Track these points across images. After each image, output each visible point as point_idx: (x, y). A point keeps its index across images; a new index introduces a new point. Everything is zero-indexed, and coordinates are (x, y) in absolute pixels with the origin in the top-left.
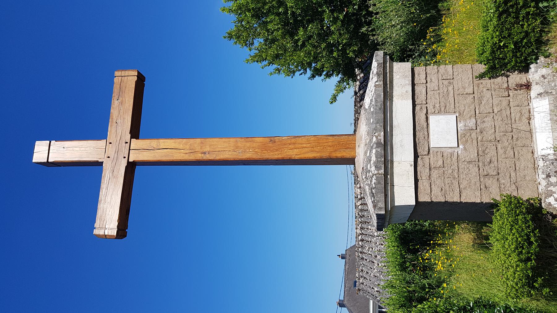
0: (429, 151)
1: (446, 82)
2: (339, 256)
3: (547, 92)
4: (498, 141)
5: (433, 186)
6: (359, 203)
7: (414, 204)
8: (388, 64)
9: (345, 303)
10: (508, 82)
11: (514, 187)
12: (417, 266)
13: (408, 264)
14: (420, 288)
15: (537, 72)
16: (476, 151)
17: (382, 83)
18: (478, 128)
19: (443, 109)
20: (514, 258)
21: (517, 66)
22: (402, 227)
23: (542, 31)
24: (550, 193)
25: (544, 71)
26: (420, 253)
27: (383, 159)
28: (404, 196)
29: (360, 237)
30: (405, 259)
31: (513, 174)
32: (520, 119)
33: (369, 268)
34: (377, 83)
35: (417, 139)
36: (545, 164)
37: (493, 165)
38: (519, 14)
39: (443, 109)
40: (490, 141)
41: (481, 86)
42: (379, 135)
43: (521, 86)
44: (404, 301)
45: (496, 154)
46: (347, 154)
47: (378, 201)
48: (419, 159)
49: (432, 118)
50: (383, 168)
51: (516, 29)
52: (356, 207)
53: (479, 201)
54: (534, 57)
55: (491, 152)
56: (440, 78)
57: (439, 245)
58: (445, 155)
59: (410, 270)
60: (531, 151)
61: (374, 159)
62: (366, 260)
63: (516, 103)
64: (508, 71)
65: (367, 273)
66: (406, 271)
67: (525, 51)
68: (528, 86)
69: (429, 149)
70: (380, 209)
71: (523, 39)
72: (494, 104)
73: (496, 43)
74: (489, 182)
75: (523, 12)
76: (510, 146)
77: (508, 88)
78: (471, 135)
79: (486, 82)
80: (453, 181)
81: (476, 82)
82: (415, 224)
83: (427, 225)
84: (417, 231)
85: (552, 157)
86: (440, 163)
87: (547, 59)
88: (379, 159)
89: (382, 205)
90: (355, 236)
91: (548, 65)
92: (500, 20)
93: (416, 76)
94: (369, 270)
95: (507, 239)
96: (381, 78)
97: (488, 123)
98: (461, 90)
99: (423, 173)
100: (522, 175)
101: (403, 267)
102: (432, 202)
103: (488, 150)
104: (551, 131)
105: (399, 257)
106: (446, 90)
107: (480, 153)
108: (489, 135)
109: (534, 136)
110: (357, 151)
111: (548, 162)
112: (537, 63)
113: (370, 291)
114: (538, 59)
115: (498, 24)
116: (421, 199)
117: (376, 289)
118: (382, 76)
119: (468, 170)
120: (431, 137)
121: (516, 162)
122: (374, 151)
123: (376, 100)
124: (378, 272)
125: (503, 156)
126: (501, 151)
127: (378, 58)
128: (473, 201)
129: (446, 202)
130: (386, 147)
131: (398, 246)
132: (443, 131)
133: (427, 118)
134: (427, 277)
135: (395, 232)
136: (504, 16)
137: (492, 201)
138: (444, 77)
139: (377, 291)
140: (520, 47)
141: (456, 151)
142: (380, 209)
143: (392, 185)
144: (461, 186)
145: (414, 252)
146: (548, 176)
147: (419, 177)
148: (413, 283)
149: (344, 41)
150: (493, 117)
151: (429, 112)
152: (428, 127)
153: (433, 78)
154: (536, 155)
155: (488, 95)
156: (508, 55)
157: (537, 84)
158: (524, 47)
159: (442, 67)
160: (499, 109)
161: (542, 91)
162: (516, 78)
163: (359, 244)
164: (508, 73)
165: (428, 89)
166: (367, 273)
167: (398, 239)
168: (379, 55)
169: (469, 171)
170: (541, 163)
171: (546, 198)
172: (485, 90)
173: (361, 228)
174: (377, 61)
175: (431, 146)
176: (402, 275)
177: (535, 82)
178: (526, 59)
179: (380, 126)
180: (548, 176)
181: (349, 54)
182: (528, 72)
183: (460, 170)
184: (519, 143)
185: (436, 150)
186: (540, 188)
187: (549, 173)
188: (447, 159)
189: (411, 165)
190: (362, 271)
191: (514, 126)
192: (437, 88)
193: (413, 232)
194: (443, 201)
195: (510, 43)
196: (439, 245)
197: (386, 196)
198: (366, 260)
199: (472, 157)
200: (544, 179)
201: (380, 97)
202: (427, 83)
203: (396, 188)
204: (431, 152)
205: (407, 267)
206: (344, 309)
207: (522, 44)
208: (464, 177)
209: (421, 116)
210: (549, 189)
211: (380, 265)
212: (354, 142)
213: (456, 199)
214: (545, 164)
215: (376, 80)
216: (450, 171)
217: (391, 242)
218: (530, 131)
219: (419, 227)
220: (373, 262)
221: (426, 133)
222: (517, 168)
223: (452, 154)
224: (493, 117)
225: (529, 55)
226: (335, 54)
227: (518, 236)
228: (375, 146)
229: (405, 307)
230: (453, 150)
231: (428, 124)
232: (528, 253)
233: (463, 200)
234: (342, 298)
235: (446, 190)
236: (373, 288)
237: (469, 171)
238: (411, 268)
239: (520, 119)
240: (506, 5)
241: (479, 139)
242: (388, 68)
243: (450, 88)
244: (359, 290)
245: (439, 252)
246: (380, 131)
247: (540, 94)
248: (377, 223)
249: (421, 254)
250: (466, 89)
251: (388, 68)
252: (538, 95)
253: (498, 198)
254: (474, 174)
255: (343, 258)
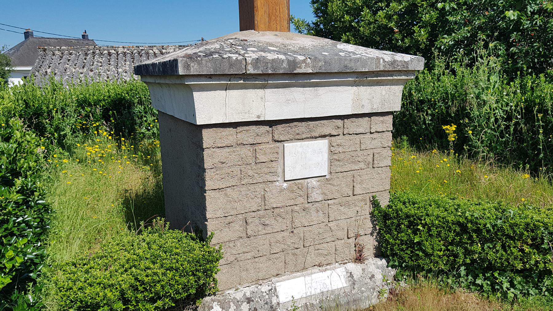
0: (278, 141)
1: (370, 159)
2: (85, 32)
3: (354, 284)
4: (292, 232)
5: (227, 150)
6: (157, 51)
7: (198, 123)
8: (404, 77)
9: (30, 39)
10: (366, 235)
11: (232, 259)
12: (86, 121)
13: (89, 109)
14: (57, 126)
15: (377, 268)
16: (279, 205)
17: (382, 68)
18: (310, 205)
19: (335, 157)
20: (125, 280)
21: (387, 245)
22: (136, 101)
23: (430, 271)
24: (226, 306)
25: (379, 277)
26: (104, 122)
27: (270, 72)
28: (210, 106)
29: (113, 51)
30: (94, 105)
31: (249, 256)
32: (320, 254)
33: (76, 62)
34: (381, 60)
35: (295, 123)
36: (264, 294)
37: (260, 229)
38: (457, 246)
39: (335, 157)
40: (292, 222)
41: (363, 203)
42: (307, 65)
43: (360, 251)
44: (34, 106)
45: (276, 231)
46: (260, 16)
47: (199, 63)
48: (267, 128)
49: (323, 143)
50: (256, 72)
51: (439, 244)
52: (151, 47)
53: (208, 216)
54: (397, 263)
55: (278, 225)
56: (375, 151)
57: (119, 147)
58: (274, 164)
59: (80, 112)
60: (280, 272)
61: (270, 56)
62: (85, 59)
63: (340, 248)
64: (379, 233)
65: (69, 60)
66: (78, 106)
67: (406, 253)
68: (359, 259)
69: (281, 141)
70: (187, 67)
71: (424, 252)
72: (339, 222)
73: (421, 220)
74: (238, 226)
75: (460, 251)
76: (286, 247)
77: (357, 236)
78: (301, 196)
79: (368, 208)
80: (236, 178)
81: (368, 197)
82: (142, 117)
83: (143, 131)
84: (133, 119)
85: (274, 301)
86: (262, 158)
87: (392, 277)
88: (270, 65)
89: (194, 69)
90: (114, 46)
91: (385, 279)
92: (453, 224)
93: (381, 118)
94: (73, 62)
95: (154, 263)
96: (399, 68)
97: (315, 217)
98: (359, 179)
99: (247, 135)
100: (248, 266)
101: (82, 103)
102: (203, 150)
103: (280, 220)
104: (309, 294)
105: (95, 98)
106: (360, 159)
107: (276, 211)
108: (301, 219)
109: (299, 274)
110: (267, 33)
111: (267, 297)
112: (387, 267)
113: (45, 63)
114: (392, 268)
115: (448, 222)
116: (206, 133)
117: (49, 71)
118: (391, 69)
119: (253, 197)
120: (299, 143)
121: (265, 257)
122: (282, 57)
123: (358, 60)
124: (72, 72)
125: (273, 240)
126: (279, 236)
127: (415, 62)
128: (207, 209)
129: (204, 170)
130: (290, 77)
131: (109, 97)
132: (306, 159)
133: (324, 136)
134: (74, 132)
135: (127, 93)
136: (458, 229)
137: (209, 233)
138: (376, 156)
139: (46, 72)
140: (413, 248)
141: (279, 179)
142: (187, 67)
143: (226, 88)
144: (228, 189)
145: (106, 117)
146: (249, 300)
147: (240, 129)
148: (63, 116)
149: (361, 29)
150: (323, 222)
151: (333, 138)
152: (313, 138)
153: (376, 141)
154: (274, 280)
155: (351, 212)
156: (403, 234)
157: (363, 270)
158: (412, 252)
159: (390, 153)
160: (333, 228)
161: (355, 277)
162: (370, 243)
163: (104, 50)
164: (375, 234)
165: (362, 136)
166: (69, 60)
167: (119, 96)
168: (416, 62)
169: (252, 199)
170: (265, 288)
171: (219, 301)
172: (357, 208)
173: (125, 53)
174: (412, 60)
175: (286, 145)
176: (72, 102)
177: (366, 267)
178: (394, 255)
179: (320, 67)
180: (249, 300)
181: (345, 34)
182: (375, 257)
183: (252, 187)
184: (291, 257)
185: (280, 151)
186: (231, 292)
187: (253, 301)
188: (268, 167)
189: (258, 117)
190: (71, 54)
191: (312, 248)
192: (363, 147)
193: (131, 115)
194: (206, 166)
195: (421, 237)
196: (119, 147)
197: (210, 77)
198: (85, 59)
199: (272, 200)
200: (245, 294)
201: (363, 67)
202: (371, 133)
203: (221, 94)
204: (278, 144)
205: (83, 108)
206: (22, 38)
207: (417, 250)
208: (243, 193)
209: (328, 127)
210: (232, 304)
211: (81, 75)
212: (279, 28)
213: (209, 184)
214: (264, 294)
215: (387, 60)
216: (250, 173)
217: (114, 89)
218: (305, 269)
219: (138, 121)
220: (83, 67)
221: (304, 136)
222: (256, 260)
223: (275, 173)
224: (323, 222)
225: (401, 258)
226: (347, 17)
227: (163, 283)
228: (291, 59)
229: (26, 107)
230: (281, 174)
231: (316, 138)
232: (137, 302)
233: (208, 195)
234: (35, 34)
235: (221, 169)
236: (50, 67)
237: (252, 199)
238: (83, 113)
239: (320, 254)
240: (474, 231)
241: (296, 208)
242: (399, 78)
243: (362, 165)
244: (45, 50)
245: (111, 147)
246: (313, 67)
247: (351, 275)
248: (153, 65)
249: (103, 124)
250: (359, 186)
251: (399, 78)
252: (351, 273)
253: (214, 241)
254: (248, 206)
255: (83, 36)
